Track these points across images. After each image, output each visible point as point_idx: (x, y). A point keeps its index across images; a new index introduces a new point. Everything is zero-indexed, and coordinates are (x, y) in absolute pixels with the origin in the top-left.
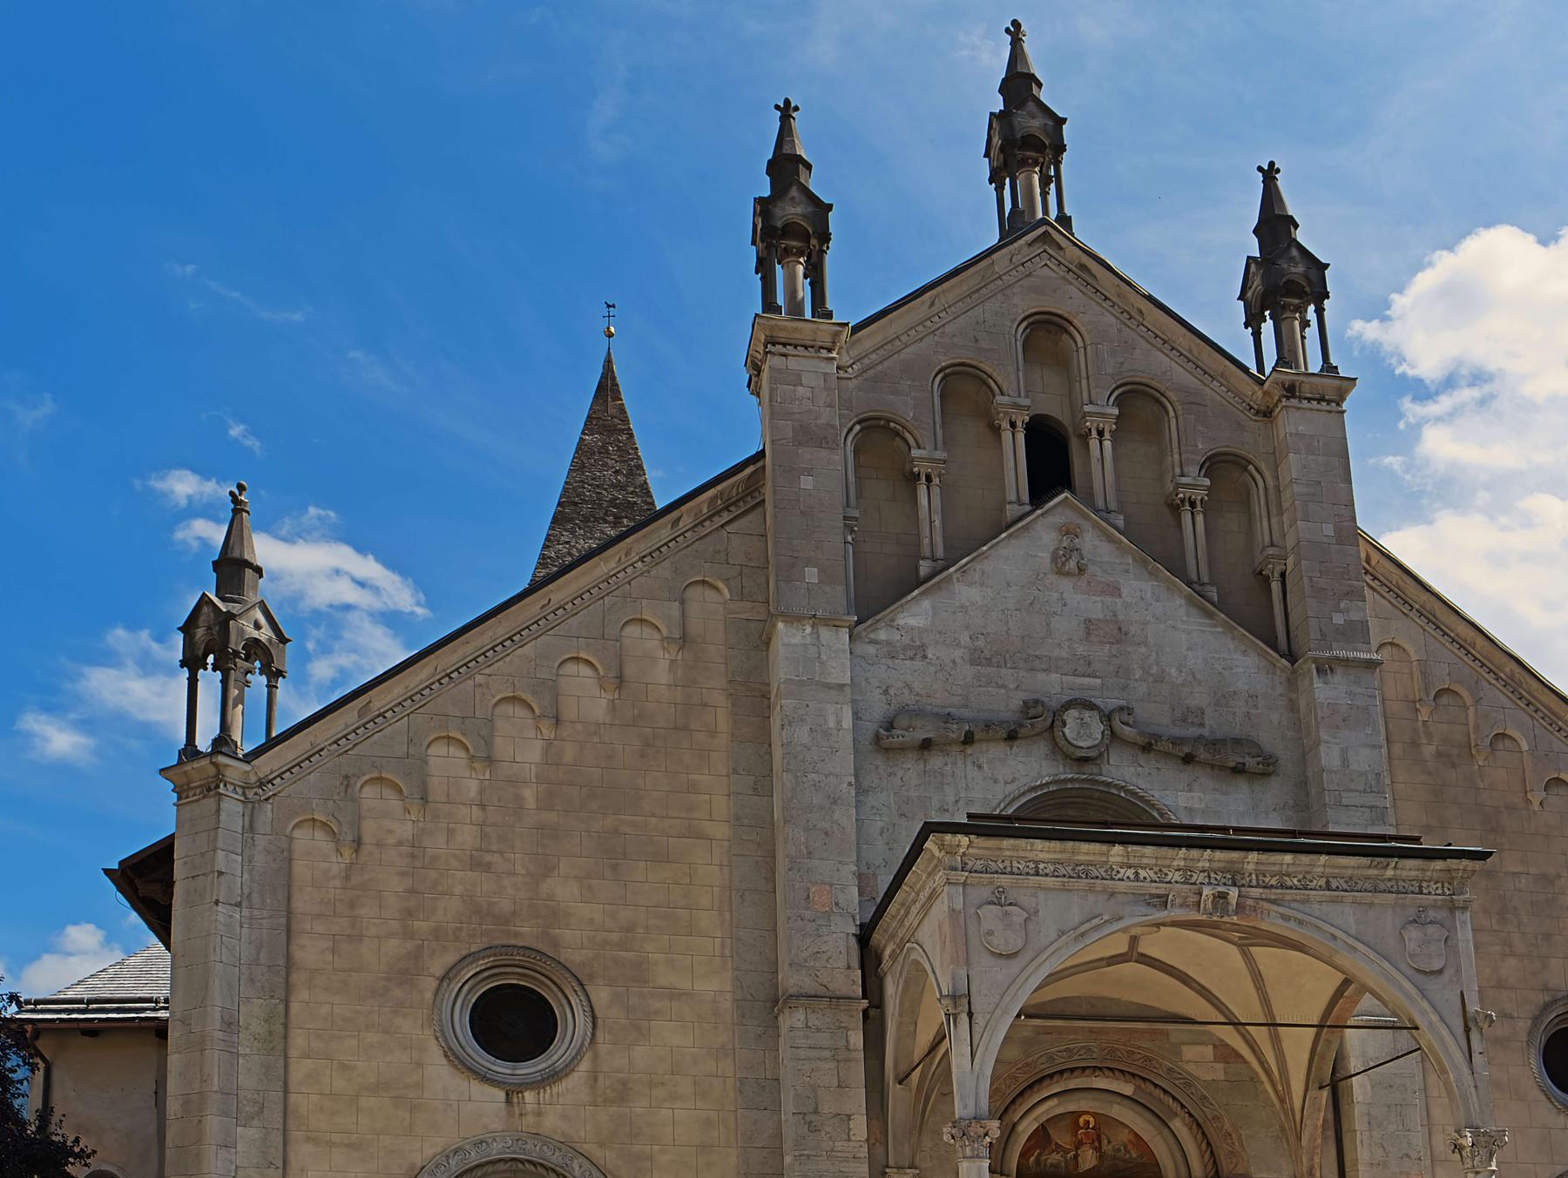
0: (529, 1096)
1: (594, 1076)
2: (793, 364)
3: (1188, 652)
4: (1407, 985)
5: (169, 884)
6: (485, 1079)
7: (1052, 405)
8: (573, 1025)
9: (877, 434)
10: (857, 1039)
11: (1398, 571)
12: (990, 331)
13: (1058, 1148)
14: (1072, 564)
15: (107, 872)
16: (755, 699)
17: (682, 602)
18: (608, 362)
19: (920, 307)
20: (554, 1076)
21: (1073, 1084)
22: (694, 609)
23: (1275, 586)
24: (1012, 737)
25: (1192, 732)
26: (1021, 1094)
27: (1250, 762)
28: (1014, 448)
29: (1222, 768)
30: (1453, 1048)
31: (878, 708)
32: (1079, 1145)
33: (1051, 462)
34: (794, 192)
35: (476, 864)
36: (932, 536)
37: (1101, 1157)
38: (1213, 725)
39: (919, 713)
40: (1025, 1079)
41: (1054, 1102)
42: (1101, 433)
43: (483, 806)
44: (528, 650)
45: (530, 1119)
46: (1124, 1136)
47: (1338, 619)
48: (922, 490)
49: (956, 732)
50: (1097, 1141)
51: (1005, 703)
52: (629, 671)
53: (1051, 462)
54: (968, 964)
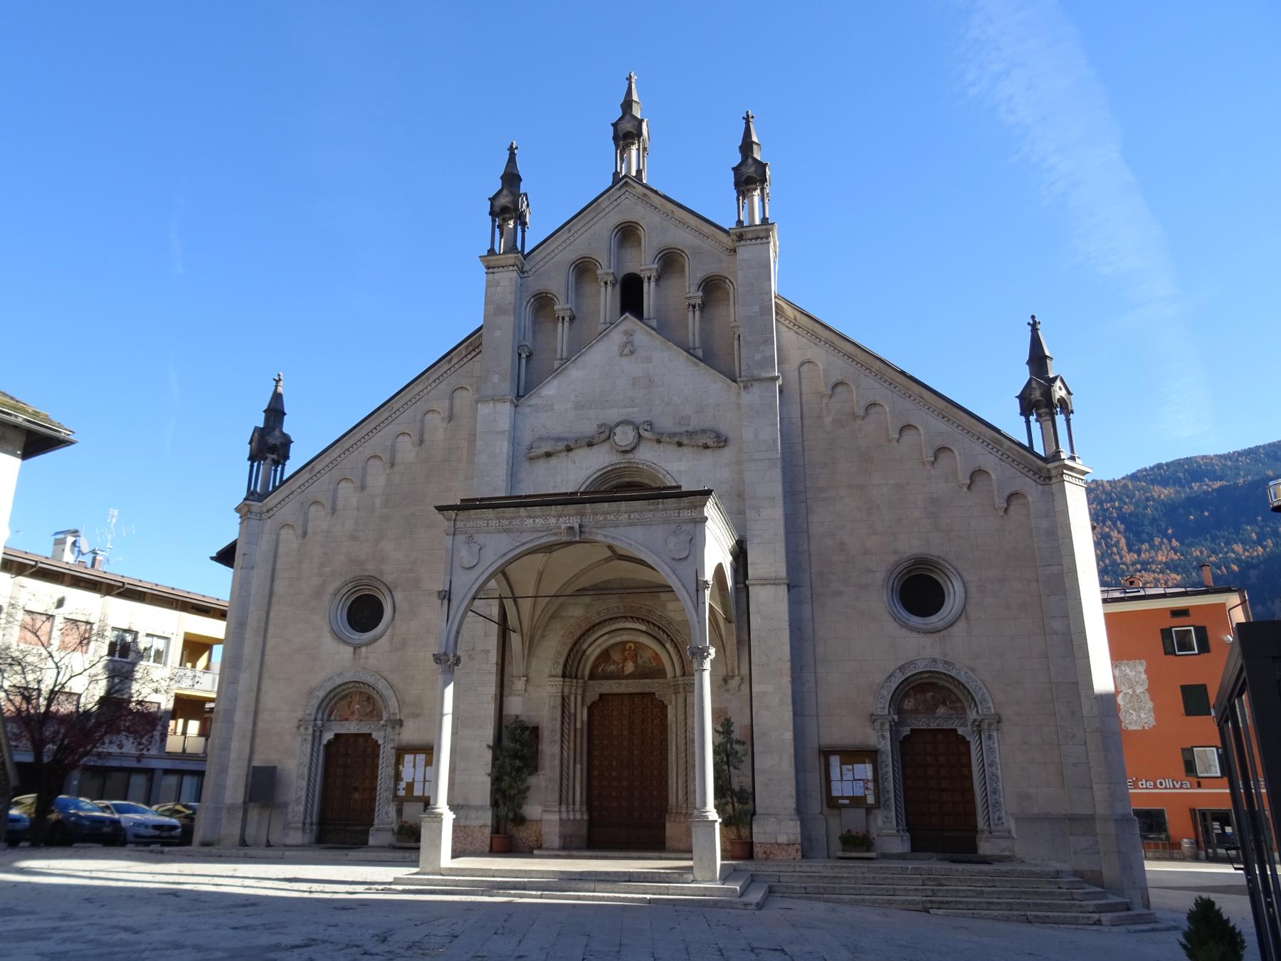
0: (363, 649)
1: (392, 636)
3: (682, 385)
6: (345, 642)
7: (631, 268)
9: (543, 302)
12: (596, 241)
14: (626, 351)
15: (212, 558)
17: (451, 399)
19: (564, 235)
21: (614, 627)
22: (457, 402)
24: (590, 445)
25: (684, 429)
26: (584, 634)
27: (710, 443)
28: (607, 299)
29: (698, 446)
30: (690, 604)
32: (625, 660)
33: (631, 295)
35: (353, 538)
37: (636, 666)
38: (695, 424)
39: (541, 439)
40: (585, 627)
41: (606, 637)
42: (649, 279)
45: (362, 661)
46: (649, 654)
47: (758, 357)
48: (560, 325)
49: (561, 446)
51: (588, 427)
52: (426, 436)
53: (631, 295)
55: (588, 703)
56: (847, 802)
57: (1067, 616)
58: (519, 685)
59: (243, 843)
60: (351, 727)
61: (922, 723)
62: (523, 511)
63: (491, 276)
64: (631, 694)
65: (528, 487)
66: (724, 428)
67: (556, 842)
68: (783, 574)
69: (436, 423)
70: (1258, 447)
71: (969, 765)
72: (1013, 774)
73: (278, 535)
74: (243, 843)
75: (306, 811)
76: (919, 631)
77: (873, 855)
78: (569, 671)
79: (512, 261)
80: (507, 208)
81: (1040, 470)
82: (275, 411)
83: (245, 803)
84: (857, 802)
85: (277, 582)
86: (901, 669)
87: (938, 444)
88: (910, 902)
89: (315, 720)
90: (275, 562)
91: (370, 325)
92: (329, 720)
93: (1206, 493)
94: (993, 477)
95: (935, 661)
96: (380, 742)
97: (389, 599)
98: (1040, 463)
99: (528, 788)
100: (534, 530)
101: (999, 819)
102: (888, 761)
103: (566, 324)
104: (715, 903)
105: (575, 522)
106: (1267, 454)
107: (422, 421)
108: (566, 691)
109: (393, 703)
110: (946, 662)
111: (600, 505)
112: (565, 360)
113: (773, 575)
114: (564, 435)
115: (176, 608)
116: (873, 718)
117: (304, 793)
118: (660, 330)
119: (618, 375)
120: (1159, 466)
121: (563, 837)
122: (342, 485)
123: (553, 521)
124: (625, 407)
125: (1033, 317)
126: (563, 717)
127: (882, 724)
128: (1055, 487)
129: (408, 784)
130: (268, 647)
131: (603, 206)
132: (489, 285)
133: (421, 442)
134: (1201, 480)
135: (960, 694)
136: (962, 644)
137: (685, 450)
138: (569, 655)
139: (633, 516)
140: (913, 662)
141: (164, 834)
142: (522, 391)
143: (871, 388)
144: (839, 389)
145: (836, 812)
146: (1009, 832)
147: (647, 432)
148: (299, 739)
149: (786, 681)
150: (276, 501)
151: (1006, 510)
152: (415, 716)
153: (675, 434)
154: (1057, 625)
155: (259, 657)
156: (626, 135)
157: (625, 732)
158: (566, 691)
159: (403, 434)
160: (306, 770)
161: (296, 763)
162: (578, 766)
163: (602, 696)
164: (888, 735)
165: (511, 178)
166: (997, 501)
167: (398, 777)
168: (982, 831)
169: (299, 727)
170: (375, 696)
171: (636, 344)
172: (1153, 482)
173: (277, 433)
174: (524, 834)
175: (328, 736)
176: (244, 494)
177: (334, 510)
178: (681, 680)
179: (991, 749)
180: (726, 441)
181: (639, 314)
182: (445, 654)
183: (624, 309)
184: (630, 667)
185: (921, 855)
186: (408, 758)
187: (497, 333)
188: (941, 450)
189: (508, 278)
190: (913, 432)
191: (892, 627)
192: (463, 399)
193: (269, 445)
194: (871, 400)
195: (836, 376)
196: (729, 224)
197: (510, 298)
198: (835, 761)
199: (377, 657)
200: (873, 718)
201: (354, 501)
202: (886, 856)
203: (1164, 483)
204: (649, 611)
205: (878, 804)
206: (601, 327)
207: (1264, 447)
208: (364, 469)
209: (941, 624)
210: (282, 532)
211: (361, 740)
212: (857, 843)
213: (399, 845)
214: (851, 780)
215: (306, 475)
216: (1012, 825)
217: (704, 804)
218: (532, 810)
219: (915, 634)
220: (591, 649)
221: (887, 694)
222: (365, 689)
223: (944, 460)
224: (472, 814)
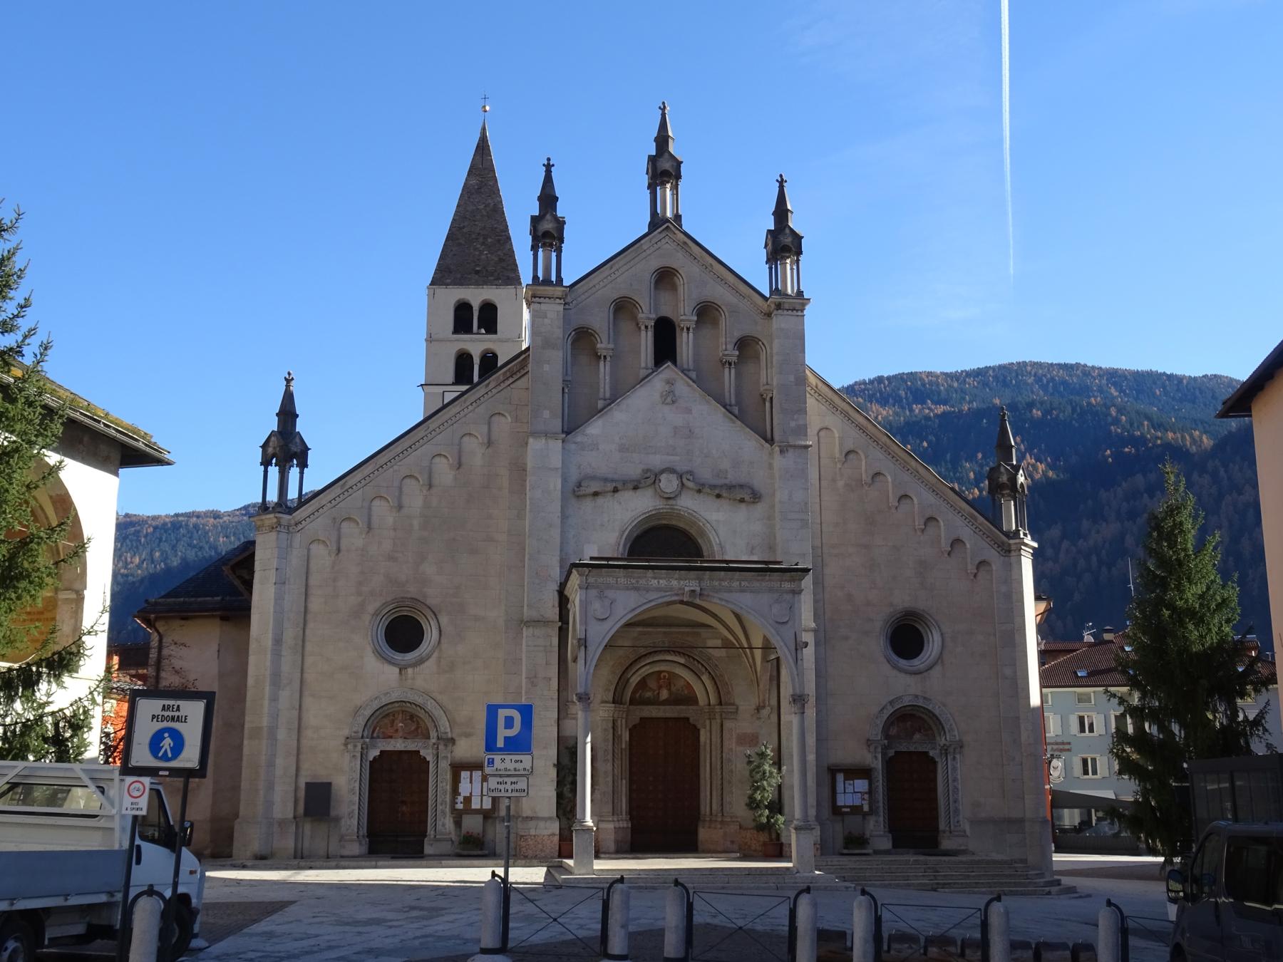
0: (410, 670)
1: (439, 658)
2: (543, 307)
3: (722, 442)
5: (252, 572)
6: (394, 664)
7: (666, 311)
8: (431, 635)
9: (582, 338)
10: (555, 641)
14: (669, 400)
15: (51, 497)
16: (519, 470)
17: (489, 424)
18: (484, 129)
20: (421, 661)
23: (768, 404)
24: (635, 488)
27: (747, 498)
28: (646, 341)
31: (574, 476)
32: (660, 687)
33: (665, 349)
35: (391, 558)
36: (605, 389)
38: (731, 477)
39: (593, 478)
42: (688, 329)
43: (395, 530)
47: (793, 424)
48: (602, 363)
49: (610, 486)
51: (633, 470)
53: (665, 349)
60: (398, 745)
61: (903, 748)
66: (757, 483)
67: (612, 847)
69: (473, 446)
70: (988, 368)
72: (967, 788)
73: (309, 550)
76: (906, 672)
77: (870, 851)
81: (1003, 543)
84: (856, 810)
86: (891, 703)
87: (927, 516)
93: (927, 418)
95: (917, 696)
98: (1005, 538)
100: (658, 589)
106: (995, 377)
114: (610, 476)
116: (869, 743)
119: (657, 420)
120: (880, 379)
121: (617, 842)
123: (674, 583)
128: (1013, 559)
129: (465, 798)
130: (307, 664)
133: (460, 465)
134: (923, 402)
136: (940, 682)
140: (900, 698)
142: (570, 428)
144: (851, 456)
148: (347, 757)
151: (975, 576)
152: (468, 735)
154: (1008, 671)
156: (663, 170)
159: (440, 455)
163: (643, 720)
164: (880, 756)
166: (970, 567)
167: (455, 791)
170: (422, 714)
171: (677, 393)
172: (871, 398)
175: (374, 753)
177: (370, 528)
178: (718, 708)
184: (664, 694)
186: (465, 775)
187: (546, 367)
188: (931, 519)
189: (554, 310)
190: (908, 501)
192: (504, 426)
194: (877, 470)
195: (849, 446)
196: (762, 284)
197: (558, 333)
198: (840, 777)
199: (422, 678)
200: (869, 743)
201: (390, 520)
202: (876, 852)
203: (884, 401)
205: (872, 811)
206: (643, 373)
207: (993, 368)
212: (855, 842)
213: (465, 853)
214: (852, 793)
215: (337, 490)
219: (903, 675)
221: (880, 723)
224: (542, 824)
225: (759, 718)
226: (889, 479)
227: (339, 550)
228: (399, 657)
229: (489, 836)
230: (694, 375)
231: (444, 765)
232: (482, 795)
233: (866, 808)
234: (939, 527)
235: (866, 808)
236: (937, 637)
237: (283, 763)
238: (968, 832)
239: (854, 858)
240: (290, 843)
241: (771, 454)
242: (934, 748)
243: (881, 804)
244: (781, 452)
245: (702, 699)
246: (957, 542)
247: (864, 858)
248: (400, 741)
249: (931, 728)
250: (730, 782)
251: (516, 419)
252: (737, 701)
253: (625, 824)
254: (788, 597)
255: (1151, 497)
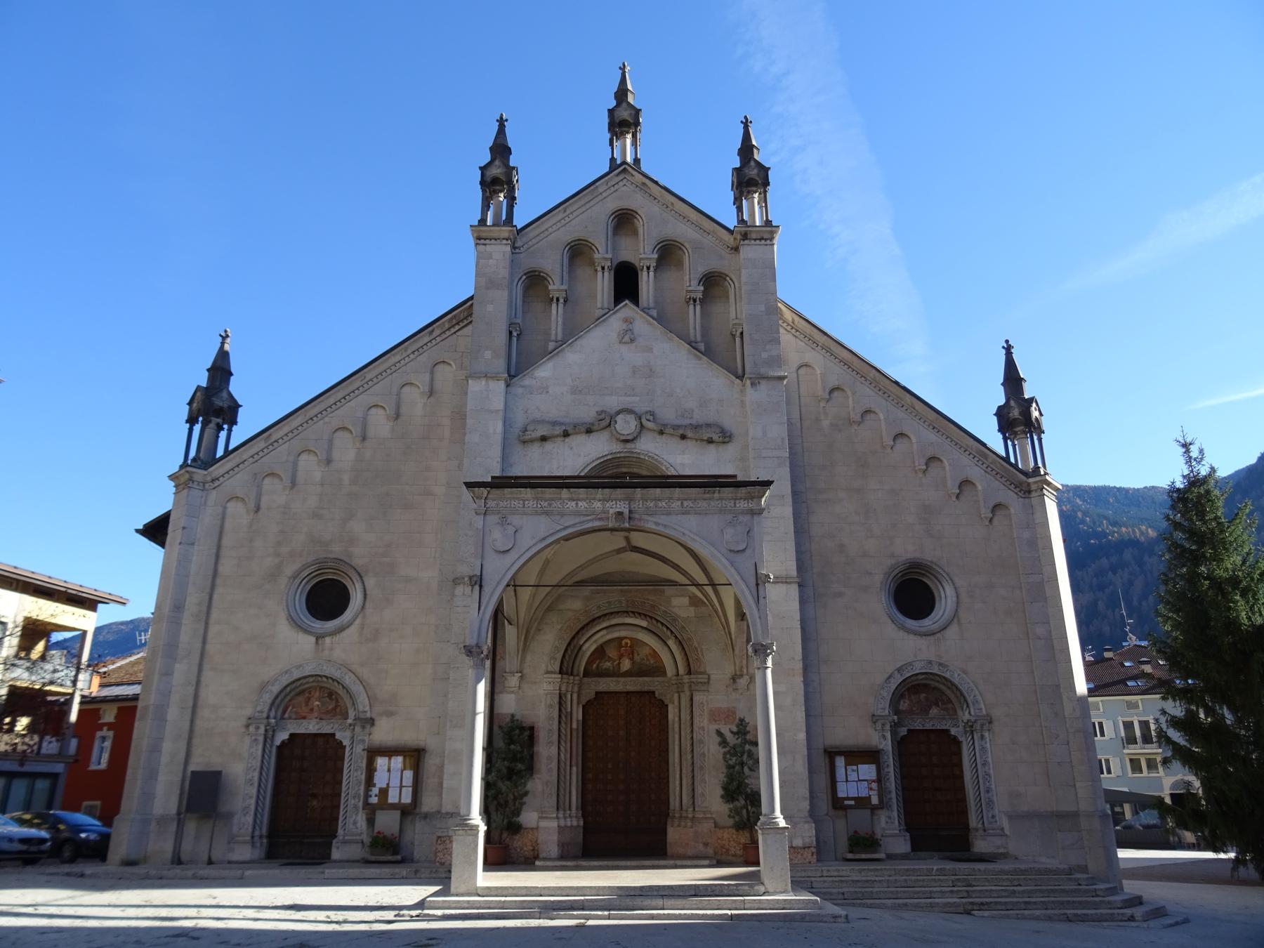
0: (328, 640)
1: (362, 627)
3: (685, 379)
4: (724, 560)
6: (306, 631)
7: (627, 255)
9: (534, 281)
11: (809, 326)
12: (592, 224)
13: (610, 659)
14: (626, 339)
15: (137, 531)
16: (460, 417)
17: (432, 373)
19: (559, 215)
20: (342, 629)
21: (614, 621)
24: (589, 431)
25: (687, 422)
26: (582, 628)
27: (715, 437)
28: (604, 285)
29: (702, 440)
32: (621, 656)
33: (626, 283)
34: (752, 163)
35: (316, 515)
36: (557, 329)
38: (699, 417)
40: (584, 620)
42: (648, 268)
43: (322, 485)
44: (352, 403)
45: (326, 652)
46: (646, 651)
47: (765, 355)
48: (554, 305)
49: (558, 430)
50: (631, 655)
51: (587, 413)
52: (403, 410)
53: (626, 283)
54: (482, 557)
55: (584, 702)
56: (852, 802)
57: (1048, 623)
58: (513, 681)
59: (177, 860)
61: (917, 725)
62: (565, 493)
63: (481, 248)
64: (628, 693)
65: (518, 470)
66: (728, 423)
67: (554, 851)
68: (794, 573)
71: (960, 765)
72: (1001, 773)
73: (225, 508)
74: (177, 860)
75: (255, 821)
76: (915, 633)
77: (882, 856)
78: (565, 669)
79: (506, 235)
80: (498, 180)
81: (1021, 483)
82: (221, 370)
83: (179, 814)
84: (862, 802)
85: (222, 561)
86: (899, 670)
87: (929, 454)
88: (951, 905)
89: (268, 717)
90: (220, 538)
91: (346, 287)
92: (282, 718)
94: (980, 487)
95: (930, 662)
96: (346, 742)
97: (358, 586)
99: (526, 793)
100: (577, 513)
101: (993, 817)
102: (890, 761)
103: (561, 305)
104: (802, 918)
105: (623, 507)
107: (398, 394)
108: (563, 689)
109: (363, 701)
110: (940, 664)
111: (652, 491)
112: (561, 343)
113: (784, 573)
115: (16, 589)
116: (874, 719)
117: (253, 801)
118: (661, 319)
119: (612, 363)
121: (562, 845)
122: (304, 457)
123: (598, 505)
124: (626, 395)
125: (1007, 341)
126: (560, 716)
127: (883, 725)
128: (1035, 501)
131: (601, 190)
132: (479, 257)
133: (397, 416)
135: (952, 697)
136: (956, 644)
137: (689, 443)
138: (566, 650)
139: (686, 503)
140: (910, 664)
141: (34, 849)
142: (515, 370)
143: (866, 396)
144: (836, 394)
145: (841, 813)
146: (1003, 829)
147: (648, 422)
148: (247, 740)
149: (799, 679)
150: (222, 471)
151: (991, 520)
152: (390, 714)
153: (679, 427)
154: (1040, 630)
155: (199, 645)
156: (623, 122)
157: (622, 733)
158: (563, 689)
160: (256, 775)
161: (245, 769)
162: (574, 769)
164: (888, 735)
165: (501, 150)
166: (983, 510)
167: (370, 782)
168: (977, 830)
169: (247, 726)
170: (341, 691)
173: (224, 394)
174: (520, 843)
175: (282, 736)
176: (181, 461)
178: (686, 679)
179: (983, 749)
180: (730, 436)
181: (635, 299)
182: (478, 646)
183: (618, 298)
184: (626, 665)
185: (923, 854)
186: (381, 762)
187: (490, 308)
188: (932, 459)
189: (500, 251)
190: (905, 440)
191: (891, 630)
192: (446, 375)
193: (213, 405)
195: (833, 382)
196: (731, 221)
197: (504, 273)
198: (840, 762)
199: (342, 648)
200: (874, 719)
201: (318, 475)
202: (890, 857)
204: (653, 606)
205: (883, 805)
206: (598, 313)
208: (331, 442)
209: (936, 626)
210: (229, 505)
211: (321, 741)
213: (373, 858)
214: (856, 781)
215: (260, 444)
216: (1005, 823)
217: (773, 810)
218: (529, 817)
219: (911, 637)
220: (587, 645)
221: (887, 694)
222: (329, 684)
223: (934, 470)
225: (736, 690)
226: (882, 416)
227: (258, 509)
228: (319, 625)
229: (408, 837)
230: (654, 313)
231: (359, 749)
232: (401, 787)
233: (875, 800)
234: (944, 468)
235: (875, 800)
236: (949, 590)
237: (171, 749)
238: (1007, 831)
239: (857, 866)
240: (167, 847)
241: (742, 392)
242: (956, 726)
243: (894, 795)
244: (752, 384)
245: (670, 671)
246: (965, 484)
247: (872, 866)
248: (314, 722)
249: (950, 701)
250: (701, 768)
251: (461, 367)
252: (708, 670)
253: (576, 821)
254: (744, 519)
255: (1115, 573)
